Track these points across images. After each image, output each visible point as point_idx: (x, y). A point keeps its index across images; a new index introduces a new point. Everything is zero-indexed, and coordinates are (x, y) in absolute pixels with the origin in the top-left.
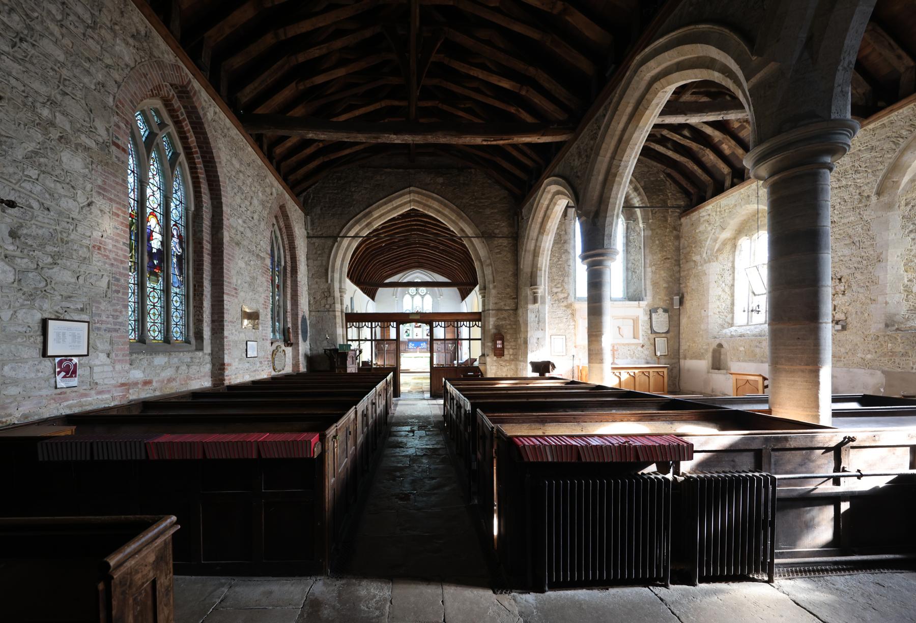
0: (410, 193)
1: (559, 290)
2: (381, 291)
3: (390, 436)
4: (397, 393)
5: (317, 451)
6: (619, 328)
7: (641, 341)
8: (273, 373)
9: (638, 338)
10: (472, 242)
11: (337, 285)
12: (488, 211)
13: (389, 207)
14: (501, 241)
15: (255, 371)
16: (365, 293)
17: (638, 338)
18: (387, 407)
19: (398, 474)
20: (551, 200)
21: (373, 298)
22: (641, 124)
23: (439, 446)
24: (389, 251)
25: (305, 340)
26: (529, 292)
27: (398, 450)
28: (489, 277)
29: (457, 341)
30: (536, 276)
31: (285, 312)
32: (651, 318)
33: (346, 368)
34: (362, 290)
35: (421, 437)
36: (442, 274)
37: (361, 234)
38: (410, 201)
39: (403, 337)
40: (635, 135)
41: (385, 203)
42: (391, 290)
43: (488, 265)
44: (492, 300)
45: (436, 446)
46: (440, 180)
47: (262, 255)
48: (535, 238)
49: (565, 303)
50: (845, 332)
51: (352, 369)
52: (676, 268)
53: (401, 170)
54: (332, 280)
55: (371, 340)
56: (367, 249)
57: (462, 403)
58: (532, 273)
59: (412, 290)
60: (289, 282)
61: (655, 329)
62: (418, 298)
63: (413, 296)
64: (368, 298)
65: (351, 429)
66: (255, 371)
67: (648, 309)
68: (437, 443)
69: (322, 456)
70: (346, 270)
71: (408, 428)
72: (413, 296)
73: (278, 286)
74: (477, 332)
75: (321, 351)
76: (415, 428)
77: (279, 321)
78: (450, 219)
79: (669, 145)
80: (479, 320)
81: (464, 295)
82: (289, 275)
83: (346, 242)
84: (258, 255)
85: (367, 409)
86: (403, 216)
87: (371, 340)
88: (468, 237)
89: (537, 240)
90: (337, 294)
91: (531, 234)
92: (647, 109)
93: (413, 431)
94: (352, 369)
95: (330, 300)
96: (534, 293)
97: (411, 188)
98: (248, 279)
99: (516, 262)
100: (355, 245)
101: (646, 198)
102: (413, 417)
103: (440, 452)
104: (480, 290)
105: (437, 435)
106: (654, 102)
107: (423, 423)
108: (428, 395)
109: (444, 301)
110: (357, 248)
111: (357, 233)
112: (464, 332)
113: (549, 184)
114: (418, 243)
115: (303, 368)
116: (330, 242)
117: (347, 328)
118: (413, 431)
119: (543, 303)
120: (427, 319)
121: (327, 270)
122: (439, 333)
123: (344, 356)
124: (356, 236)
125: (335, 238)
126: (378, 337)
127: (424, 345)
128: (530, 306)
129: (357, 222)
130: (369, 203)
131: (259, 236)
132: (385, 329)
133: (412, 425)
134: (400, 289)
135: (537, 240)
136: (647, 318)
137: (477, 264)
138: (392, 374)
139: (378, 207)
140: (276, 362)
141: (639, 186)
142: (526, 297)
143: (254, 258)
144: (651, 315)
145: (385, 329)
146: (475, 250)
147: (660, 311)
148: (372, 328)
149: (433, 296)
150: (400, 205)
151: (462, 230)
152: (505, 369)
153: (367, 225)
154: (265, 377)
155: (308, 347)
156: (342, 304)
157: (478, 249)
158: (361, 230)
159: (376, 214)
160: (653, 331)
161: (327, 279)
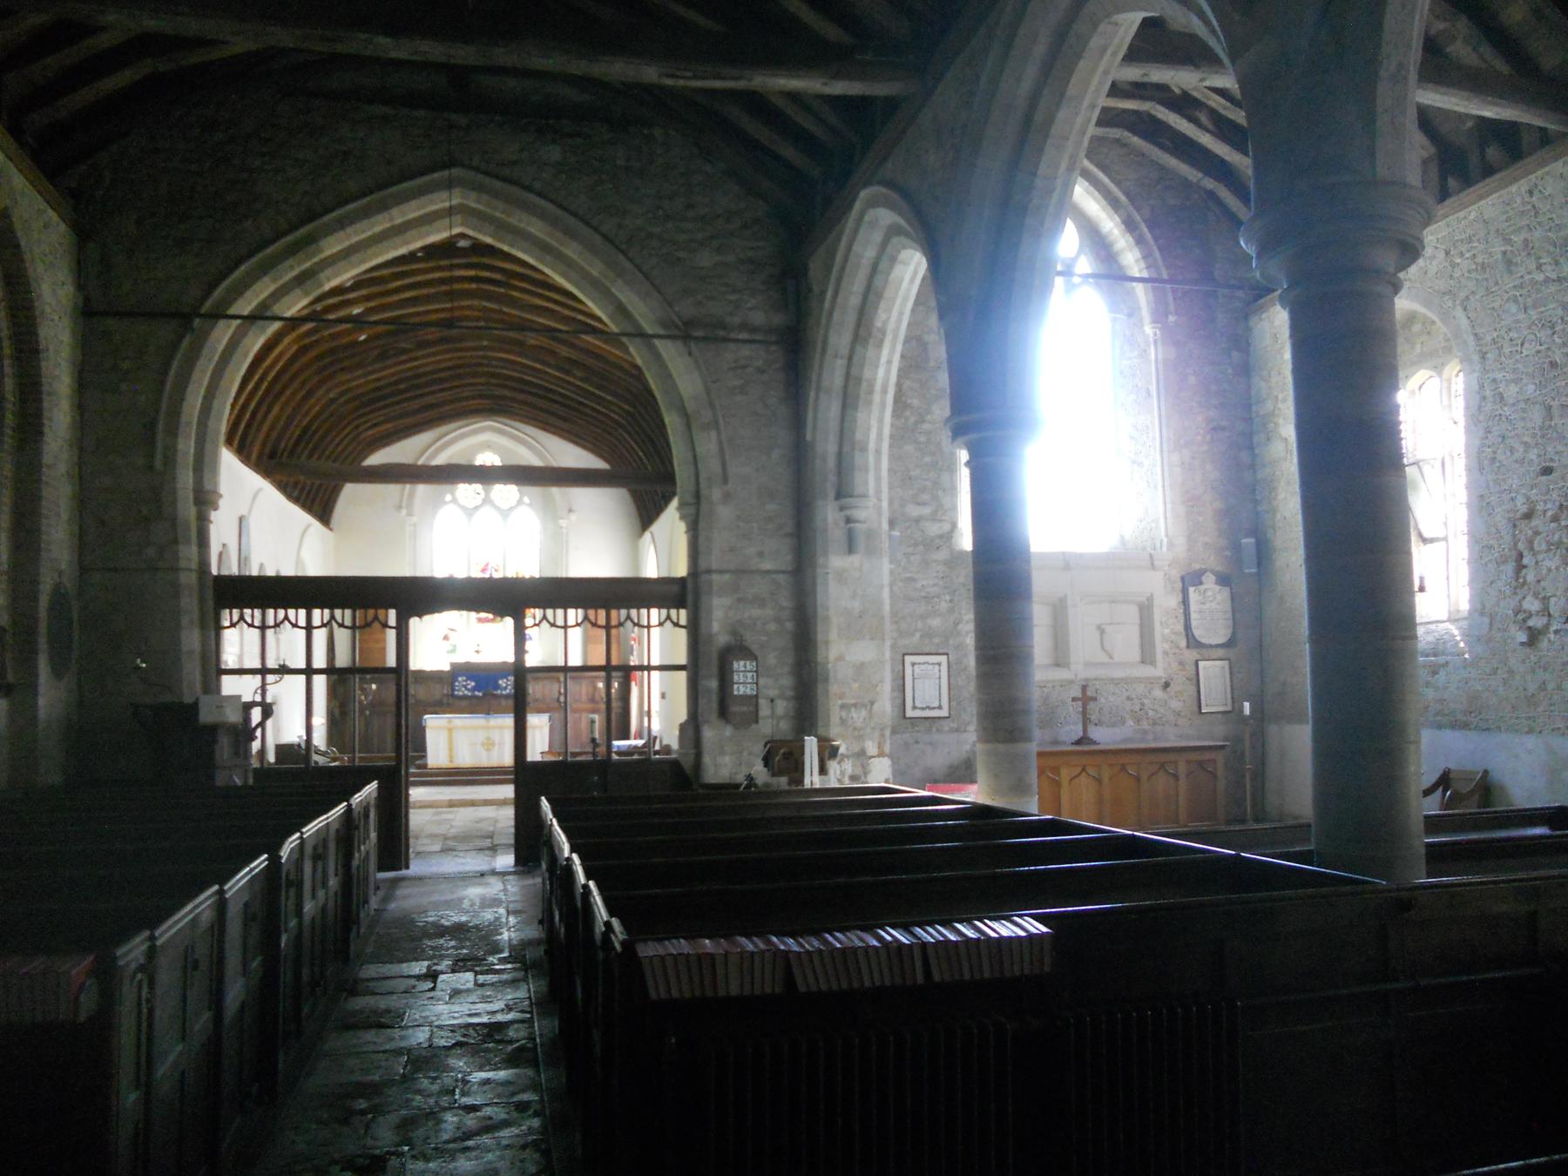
0: (449, 185)
1: (927, 511)
2: (352, 496)
3: (353, 993)
4: (394, 847)
5: (88, 1003)
6: (1102, 632)
7: (1159, 671)
9: (1153, 663)
10: (658, 357)
12: (706, 259)
13: (379, 224)
14: (746, 351)
16: (295, 500)
17: (1153, 663)
19: (362, 1104)
20: (884, 246)
22: (1072, 90)
23: (510, 1016)
24: (383, 356)
25: (58, 672)
27: (370, 1035)
29: (621, 673)
32: (1185, 602)
34: (283, 487)
38: (450, 212)
40: (1061, 115)
41: (366, 213)
42: (391, 490)
43: (706, 427)
45: (500, 1018)
46: (554, 153)
48: (845, 351)
49: (942, 555)
50: (1528, 650)
52: (1245, 456)
53: (421, 113)
55: (309, 672)
56: (304, 350)
59: (467, 492)
61: (1197, 633)
65: (202, 951)
67: (1176, 574)
69: (104, 1020)
78: (586, 276)
79: (1204, 119)
80: (680, 603)
83: (223, 333)
86: (431, 251)
87: (309, 672)
88: (642, 335)
89: (850, 358)
91: (833, 339)
92: (1079, 56)
96: (848, 520)
97: (456, 172)
99: (798, 422)
100: (255, 342)
101: (1157, 254)
103: (511, 1033)
106: (1095, 43)
108: (506, 860)
110: (268, 347)
111: (264, 306)
113: (873, 203)
120: (504, 598)
121: (151, 426)
125: (188, 318)
126: (342, 660)
129: (265, 269)
130: (311, 215)
134: (421, 489)
135: (850, 358)
136: (1173, 601)
137: (671, 420)
138: (374, 785)
139: (342, 224)
141: (1138, 218)
144: (1185, 592)
146: (667, 376)
147: (1209, 581)
148: (309, 628)
149: (550, 513)
150: (428, 219)
151: (621, 311)
153: (302, 280)
157: (678, 374)
159: (332, 245)
160: (1193, 642)
161: (151, 456)
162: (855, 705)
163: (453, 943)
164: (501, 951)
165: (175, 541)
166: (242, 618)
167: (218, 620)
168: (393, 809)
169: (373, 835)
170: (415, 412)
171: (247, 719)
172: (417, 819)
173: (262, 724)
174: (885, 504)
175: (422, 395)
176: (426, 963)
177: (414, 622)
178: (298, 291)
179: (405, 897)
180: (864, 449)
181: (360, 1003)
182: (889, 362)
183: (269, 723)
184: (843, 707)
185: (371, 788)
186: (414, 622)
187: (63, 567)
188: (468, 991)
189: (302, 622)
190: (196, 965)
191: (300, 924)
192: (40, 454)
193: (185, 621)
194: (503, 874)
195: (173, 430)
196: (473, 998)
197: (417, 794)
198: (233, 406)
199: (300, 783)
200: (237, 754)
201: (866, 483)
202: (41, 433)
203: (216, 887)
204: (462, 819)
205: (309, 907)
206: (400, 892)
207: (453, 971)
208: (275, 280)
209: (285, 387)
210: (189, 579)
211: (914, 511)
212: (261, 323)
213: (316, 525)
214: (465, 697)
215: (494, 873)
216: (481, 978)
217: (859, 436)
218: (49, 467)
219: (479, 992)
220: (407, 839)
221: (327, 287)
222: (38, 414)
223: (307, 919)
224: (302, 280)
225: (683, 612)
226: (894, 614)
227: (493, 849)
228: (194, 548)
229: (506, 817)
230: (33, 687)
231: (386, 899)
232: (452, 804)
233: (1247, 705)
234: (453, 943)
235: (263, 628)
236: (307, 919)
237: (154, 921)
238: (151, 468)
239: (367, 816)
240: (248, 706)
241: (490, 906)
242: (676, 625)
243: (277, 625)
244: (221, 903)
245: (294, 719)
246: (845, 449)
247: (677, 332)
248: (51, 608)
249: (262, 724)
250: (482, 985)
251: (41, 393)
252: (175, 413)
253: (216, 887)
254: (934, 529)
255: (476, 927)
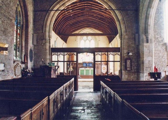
1: (159, 36)
2: (70, 38)
4: (76, 89)
8: (15, 77)
11: (47, 34)
15: (5, 75)
18: (71, 94)
21: (66, 42)
24: (74, 18)
25: (31, 61)
26: (144, 37)
28: (123, 30)
29: (107, 62)
30: (148, 29)
31: (22, 47)
33: (51, 75)
35: (88, 113)
36: (99, 30)
37: (60, 9)
39: (80, 61)
44: (125, 41)
47: (11, 18)
49: (162, 43)
51: (53, 76)
54: (45, 31)
55: (64, 61)
56: (63, 17)
57: (112, 96)
58: (145, 27)
59: (85, 37)
60: (24, 32)
62: (88, 41)
63: (85, 41)
64: (63, 42)
65: (45, 111)
66: (5, 75)
68: (97, 117)
70: (52, 26)
71: (81, 108)
72: (85, 41)
73: (19, 34)
74: (118, 58)
75: (39, 66)
76: (86, 108)
77: (19, 51)
80: (119, 51)
81: (110, 40)
82: (24, 29)
83: (52, 13)
84: (9, 18)
85: (63, 92)
87: (64, 61)
90: (47, 38)
93: (84, 110)
94: (53, 76)
95: (44, 41)
98: (3, 29)
100: (57, 14)
102: (84, 102)
104: (119, 36)
105: (97, 112)
107: (90, 105)
108: (92, 90)
109: (102, 42)
112: (111, 58)
114: (88, 15)
115: (56, 77)
116: (44, 13)
117: (52, 55)
118: (84, 110)
119: (151, 42)
120: (93, 51)
121: (43, 26)
122: (98, 58)
123: (50, 68)
124: (58, 10)
125: (47, 11)
127: (91, 65)
128: (145, 44)
131: (10, 9)
132: (71, 56)
133: (84, 106)
134: (79, 37)
140: (16, 72)
142: (143, 39)
143: (7, 19)
145: (71, 56)
146: (116, 16)
152: (132, 77)
153: (63, 5)
154: (10, 79)
155: (33, 65)
156: (50, 43)
158: (61, 6)
162: (148, 67)
163: (86, 104)
164: (94, 106)
165: (46, 43)
166: (55, 54)
167: (52, 54)
168: (76, 82)
169: (73, 86)
170: (78, 27)
171: (56, 68)
172: (79, 84)
173: (57, 69)
174: (153, 35)
175: (79, 24)
176: (82, 107)
177: (79, 54)
178: (63, 6)
179: (78, 95)
180: (150, 26)
181: (73, 114)
182: (154, 11)
183: (59, 69)
184: (146, 68)
185: (73, 79)
186: (79, 54)
187: (31, 46)
188: (90, 113)
189: (63, 54)
190: (43, 114)
191: (63, 101)
192: (28, 30)
193: (47, 54)
194: (92, 92)
195: (46, 27)
196: (91, 115)
197: (79, 80)
198: (53, 26)
199: (63, 78)
200: (54, 73)
201: (150, 31)
202: (28, 27)
203: (48, 97)
204: (85, 84)
205: (64, 98)
206: (77, 95)
207: (87, 109)
208: (59, 5)
209: (61, 23)
210: (48, 47)
211: (157, 36)
212: (57, 11)
213: (65, 43)
214: (85, 67)
215: (90, 92)
216: (92, 111)
217: (149, 24)
218: (29, 32)
219: (92, 113)
220: (78, 86)
221: (66, 6)
222: (28, 25)
223: (64, 100)
224: (63, 5)
225: (119, 53)
226: (155, 53)
227: (90, 88)
228: (48, 44)
229: (92, 84)
230: (27, 63)
231: (75, 95)
232: (83, 81)
233: (157, 76)
234: (86, 104)
235: (58, 55)
236: (64, 100)
237: (49, 95)
238: (43, 32)
239: (73, 83)
240: (56, 66)
241: (91, 98)
242: (118, 55)
243: (60, 55)
244: (49, 100)
245: (62, 69)
246: (147, 26)
247: (118, 9)
248: (30, 52)
249: (57, 69)
250: (92, 112)
251: (28, 22)
252: (46, 25)
253: (48, 97)
254: (160, 39)
255: (89, 101)
